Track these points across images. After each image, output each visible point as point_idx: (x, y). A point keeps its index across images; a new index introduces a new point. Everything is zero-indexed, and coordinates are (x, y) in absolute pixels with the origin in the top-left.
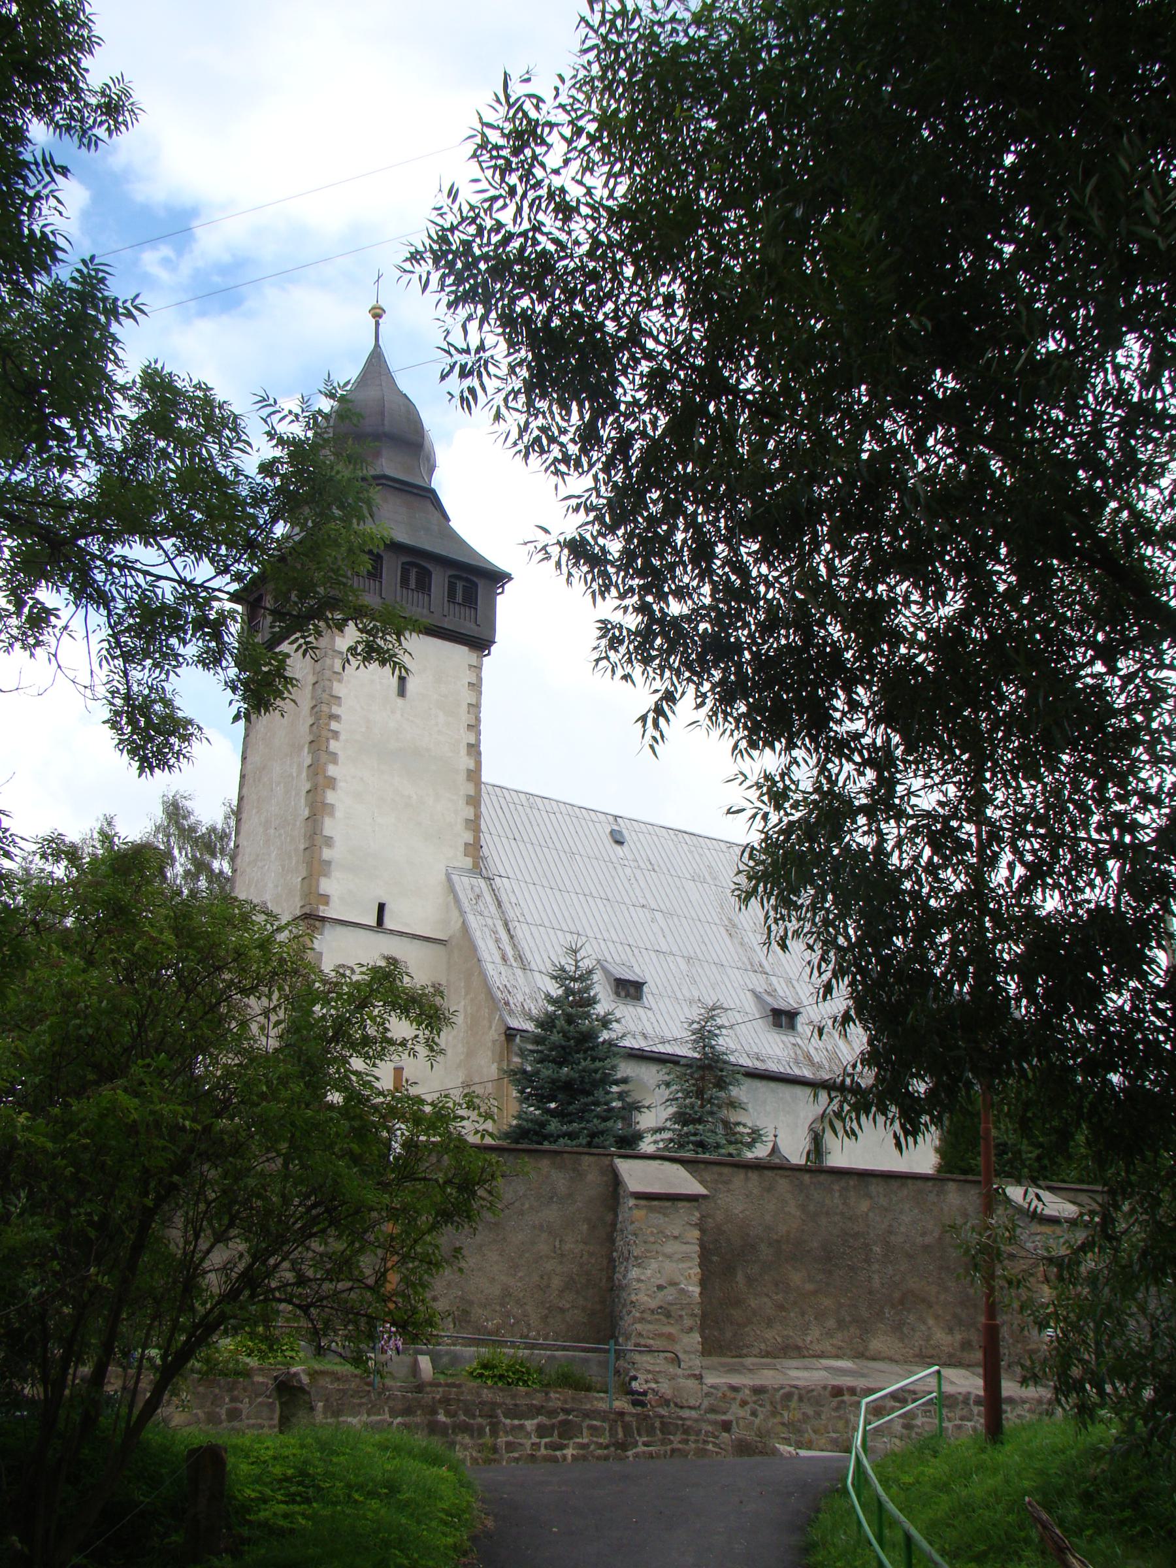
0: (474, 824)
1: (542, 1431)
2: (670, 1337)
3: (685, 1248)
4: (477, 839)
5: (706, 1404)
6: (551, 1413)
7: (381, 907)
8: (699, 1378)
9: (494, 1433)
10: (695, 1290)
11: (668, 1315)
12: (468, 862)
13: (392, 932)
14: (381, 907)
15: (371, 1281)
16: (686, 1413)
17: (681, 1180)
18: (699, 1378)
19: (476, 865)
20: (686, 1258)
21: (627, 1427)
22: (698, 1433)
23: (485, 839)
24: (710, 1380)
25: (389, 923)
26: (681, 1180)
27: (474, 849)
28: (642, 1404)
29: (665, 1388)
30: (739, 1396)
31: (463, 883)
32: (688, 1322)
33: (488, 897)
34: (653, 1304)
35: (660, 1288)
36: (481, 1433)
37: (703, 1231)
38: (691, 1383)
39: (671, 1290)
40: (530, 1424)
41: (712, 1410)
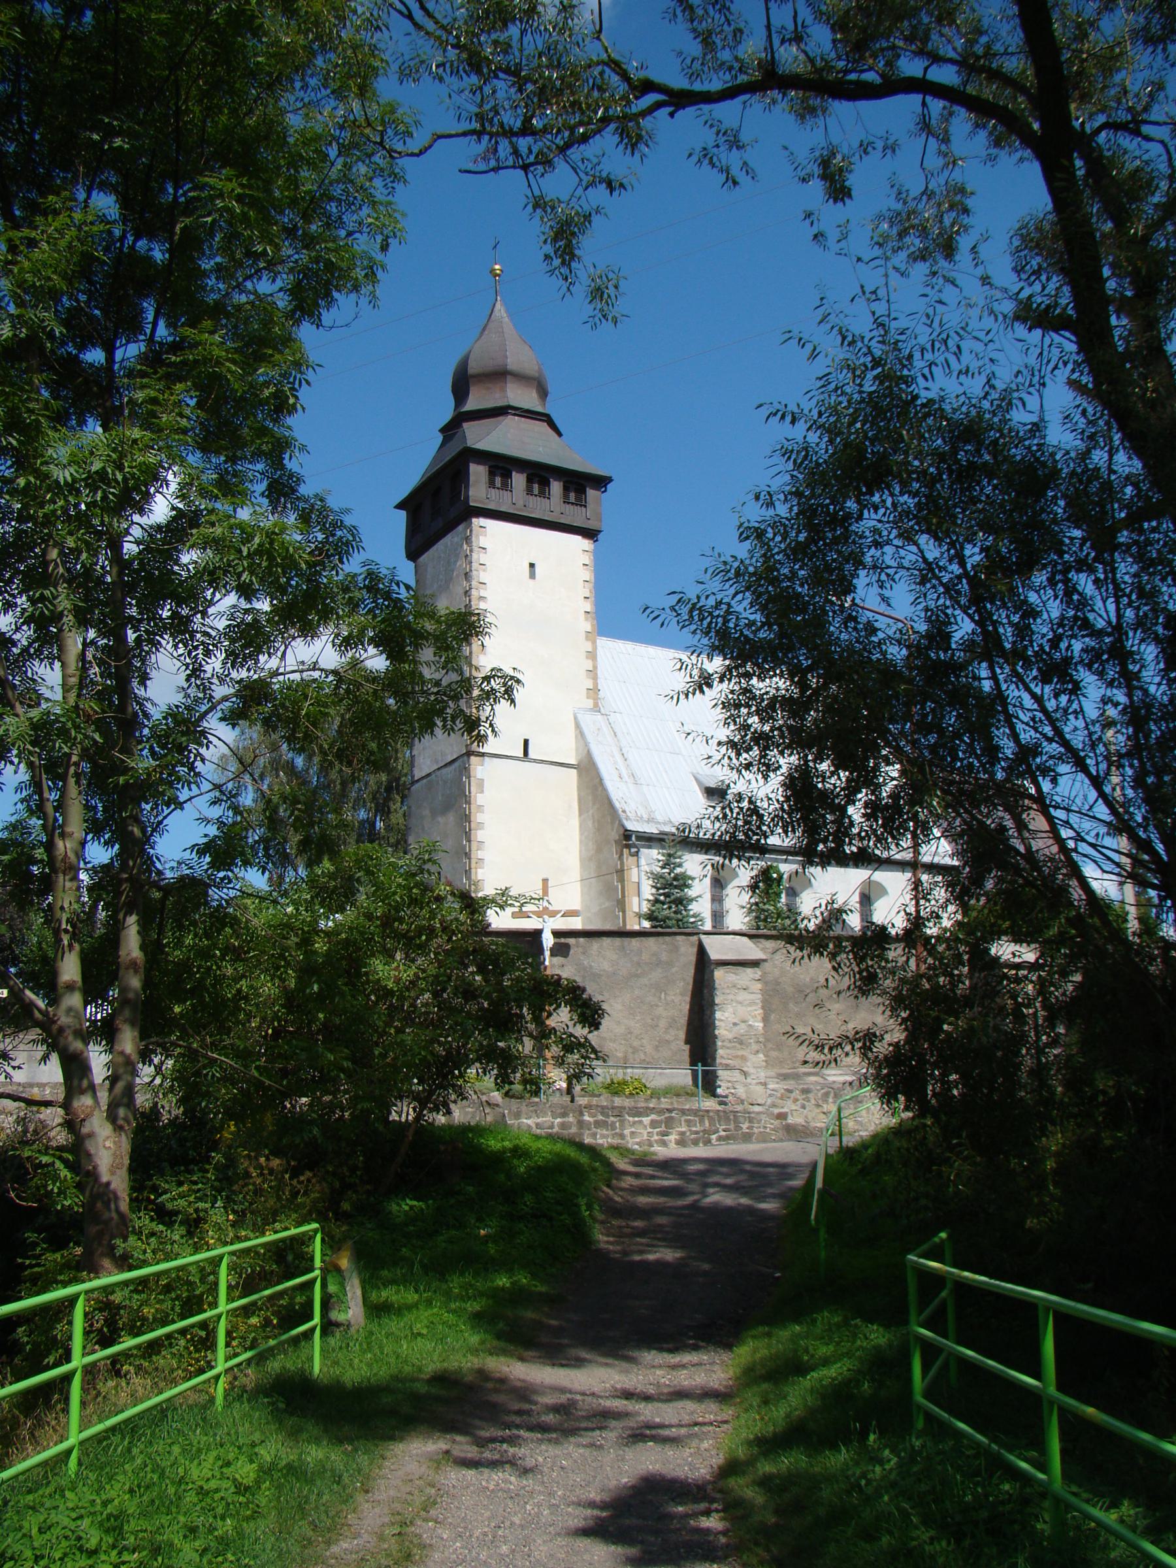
0: (593, 673)
1: (654, 1124)
2: (743, 1058)
3: (752, 997)
4: (596, 684)
5: (769, 1101)
6: (660, 1112)
7: (526, 742)
8: (765, 1084)
9: (622, 1127)
10: (760, 1025)
11: (741, 1043)
12: (590, 703)
13: (535, 761)
14: (526, 742)
15: (1072, 575)
16: (757, 1109)
17: (750, 950)
18: (765, 1084)
19: (596, 705)
20: (752, 1003)
21: (711, 1119)
22: (759, 1121)
23: (602, 684)
24: (771, 1086)
25: (532, 754)
26: (750, 950)
27: (594, 692)
28: (725, 1103)
29: (741, 1091)
30: (793, 1095)
31: (589, 722)
32: (755, 1047)
33: (605, 729)
34: (730, 1036)
35: (735, 1024)
36: (614, 1128)
37: (766, 983)
38: (760, 1088)
39: (743, 1025)
40: (646, 1120)
41: (774, 1105)
